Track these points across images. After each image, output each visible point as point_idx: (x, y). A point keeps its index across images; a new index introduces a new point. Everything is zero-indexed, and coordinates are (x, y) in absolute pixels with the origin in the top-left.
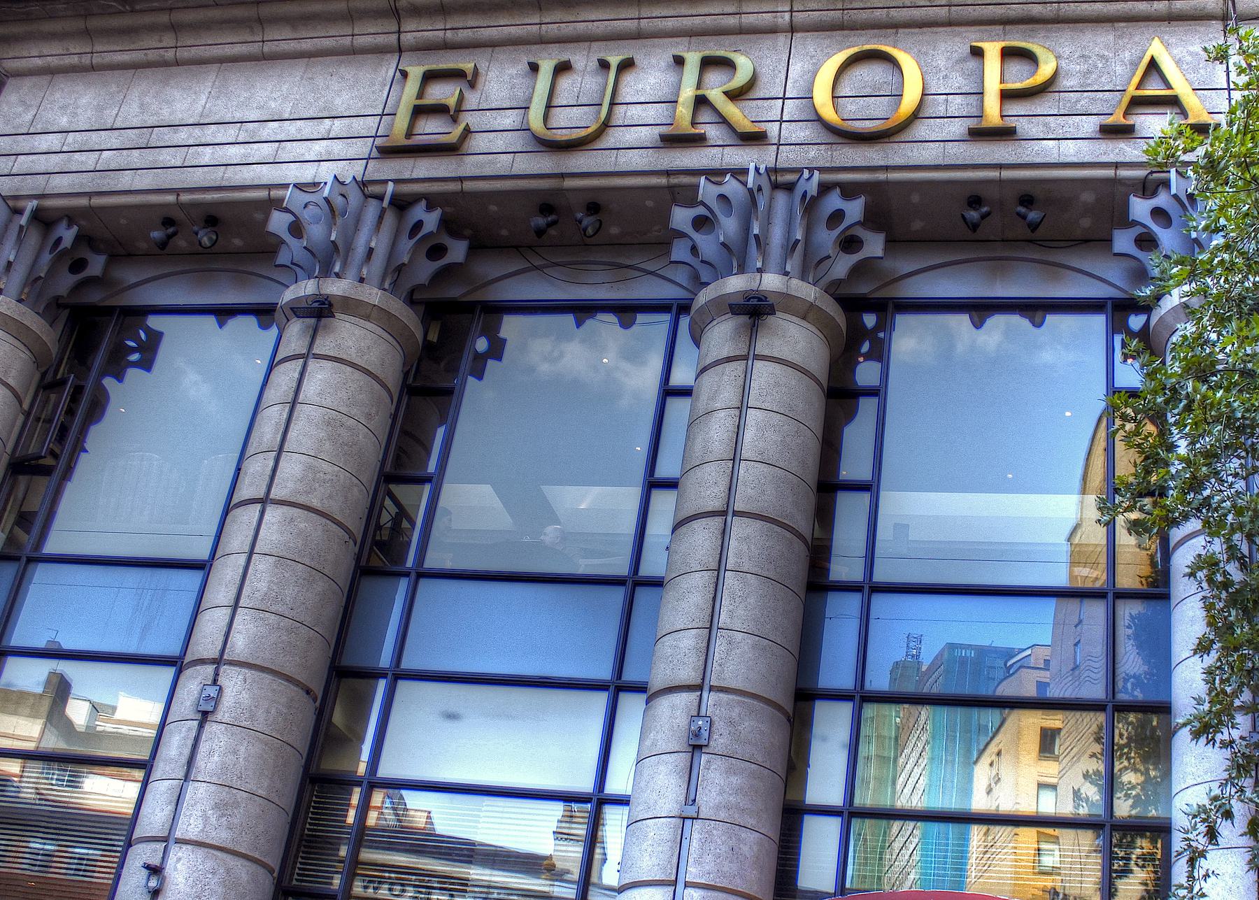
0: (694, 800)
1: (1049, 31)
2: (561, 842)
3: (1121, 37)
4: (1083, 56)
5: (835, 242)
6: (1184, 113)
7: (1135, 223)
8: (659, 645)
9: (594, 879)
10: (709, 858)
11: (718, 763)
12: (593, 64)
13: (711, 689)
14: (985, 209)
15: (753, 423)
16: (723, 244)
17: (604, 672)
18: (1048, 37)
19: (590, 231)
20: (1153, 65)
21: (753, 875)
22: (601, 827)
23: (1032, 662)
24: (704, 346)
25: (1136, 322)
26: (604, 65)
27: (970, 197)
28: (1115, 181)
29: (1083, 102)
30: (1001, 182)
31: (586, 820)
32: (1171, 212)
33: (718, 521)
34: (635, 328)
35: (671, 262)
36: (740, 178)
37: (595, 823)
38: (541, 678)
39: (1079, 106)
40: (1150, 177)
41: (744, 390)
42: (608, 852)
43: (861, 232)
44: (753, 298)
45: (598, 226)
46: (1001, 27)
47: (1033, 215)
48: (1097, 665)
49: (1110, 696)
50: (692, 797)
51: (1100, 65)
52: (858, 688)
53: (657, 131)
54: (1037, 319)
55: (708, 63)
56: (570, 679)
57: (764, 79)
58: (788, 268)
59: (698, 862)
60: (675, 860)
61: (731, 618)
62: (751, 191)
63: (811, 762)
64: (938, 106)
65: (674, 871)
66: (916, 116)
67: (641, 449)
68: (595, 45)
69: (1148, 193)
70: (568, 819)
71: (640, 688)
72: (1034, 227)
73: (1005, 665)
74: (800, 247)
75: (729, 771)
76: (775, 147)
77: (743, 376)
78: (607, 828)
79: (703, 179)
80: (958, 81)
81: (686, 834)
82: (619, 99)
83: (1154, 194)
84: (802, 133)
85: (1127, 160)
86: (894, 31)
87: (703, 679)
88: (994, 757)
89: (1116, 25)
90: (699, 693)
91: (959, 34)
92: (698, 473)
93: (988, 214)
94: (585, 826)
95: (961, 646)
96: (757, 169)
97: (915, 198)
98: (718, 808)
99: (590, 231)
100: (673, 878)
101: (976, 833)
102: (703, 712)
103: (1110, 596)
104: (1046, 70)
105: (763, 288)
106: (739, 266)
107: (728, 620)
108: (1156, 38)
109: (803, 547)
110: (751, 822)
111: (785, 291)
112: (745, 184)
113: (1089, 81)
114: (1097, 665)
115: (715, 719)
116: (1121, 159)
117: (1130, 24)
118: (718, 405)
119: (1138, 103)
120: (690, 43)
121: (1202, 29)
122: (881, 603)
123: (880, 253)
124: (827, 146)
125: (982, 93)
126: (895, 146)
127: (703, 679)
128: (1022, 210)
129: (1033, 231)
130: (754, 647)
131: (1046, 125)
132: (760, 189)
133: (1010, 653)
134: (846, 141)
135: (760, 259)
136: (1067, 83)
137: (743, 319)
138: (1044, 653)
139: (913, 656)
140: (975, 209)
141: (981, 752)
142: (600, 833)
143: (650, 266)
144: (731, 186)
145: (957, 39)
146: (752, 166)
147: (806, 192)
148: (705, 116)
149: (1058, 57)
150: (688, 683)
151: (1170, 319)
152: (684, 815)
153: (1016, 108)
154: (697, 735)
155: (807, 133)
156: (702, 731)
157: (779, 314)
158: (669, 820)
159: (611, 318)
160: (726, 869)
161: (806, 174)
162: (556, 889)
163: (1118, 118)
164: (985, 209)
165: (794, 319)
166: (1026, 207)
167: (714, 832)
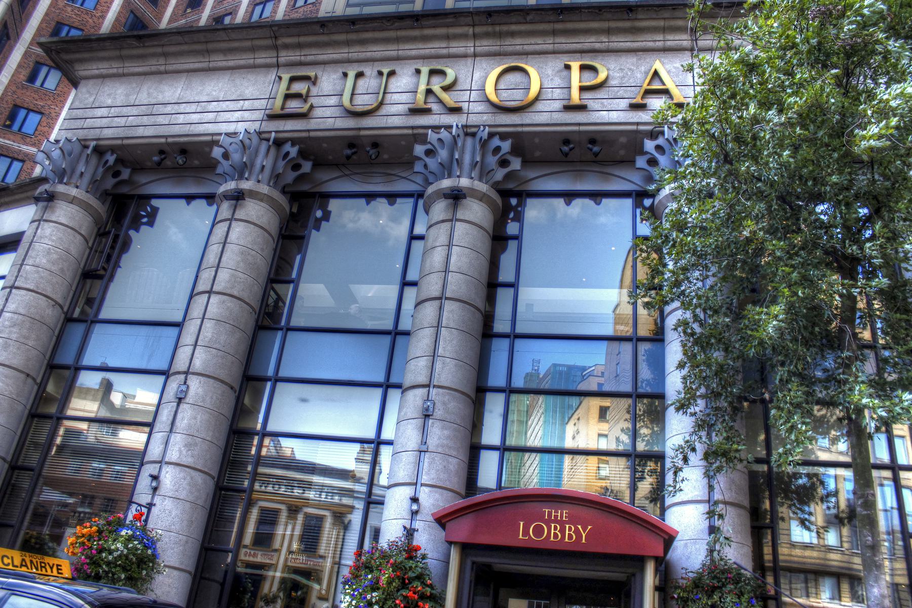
1: (603, 56)
3: (640, 59)
4: (621, 69)
6: (671, 98)
7: (647, 153)
9: (375, 482)
10: (433, 472)
11: (438, 424)
12: (375, 73)
13: (434, 386)
14: (572, 146)
16: (440, 163)
19: (373, 157)
20: (656, 73)
21: (455, 480)
26: (380, 73)
28: (637, 132)
30: (580, 132)
33: (437, 303)
37: (376, 454)
43: (509, 157)
47: (596, 149)
53: (407, 106)
54: (598, 201)
55: (432, 72)
57: (461, 81)
58: (473, 175)
59: (428, 474)
61: (444, 351)
62: (454, 137)
66: (537, 99)
67: (399, 266)
68: (376, 63)
71: (398, 386)
72: (596, 155)
74: (479, 165)
75: (443, 428)
78: (382, 456)
79: (430, 131)
81: (422, 459)
82: (388, 91)
85: (643, 121)
88: (576, 421)
91: (558, 58)
93: (573, 148)
95: (560, 365)
96: (457, 126)
97: (537, 140)
98: (437, 446)
99: (373, 157)
101: (567, 458)
102: (430, 398)
104: (602, 76)
105: (460, 185)
108: (658, 61)
110: (454, 453)
112: (451, 133)
122: (519, 343)
126: (527, 114)
128: (590, 146)
130: (456, 365)
131: (602, 103)
132: (458, 136)
133: (584, 369)
137: (450, 201)
138: (601, 369)
140: (567, 146)
141: (570, 419)
143: (403, 175)
144: (444, 134)
147: (481, 137)
148: (431, 99)
149: (608, 70)
151: (664, 201)
154: (427, 409)
157: (468, 198)
159: (384, 200)
160: (441, 477)
161: (482, 128)
162: (356, 487)
163: (638, 100)
164: (572, 146)
165: (476, 201)
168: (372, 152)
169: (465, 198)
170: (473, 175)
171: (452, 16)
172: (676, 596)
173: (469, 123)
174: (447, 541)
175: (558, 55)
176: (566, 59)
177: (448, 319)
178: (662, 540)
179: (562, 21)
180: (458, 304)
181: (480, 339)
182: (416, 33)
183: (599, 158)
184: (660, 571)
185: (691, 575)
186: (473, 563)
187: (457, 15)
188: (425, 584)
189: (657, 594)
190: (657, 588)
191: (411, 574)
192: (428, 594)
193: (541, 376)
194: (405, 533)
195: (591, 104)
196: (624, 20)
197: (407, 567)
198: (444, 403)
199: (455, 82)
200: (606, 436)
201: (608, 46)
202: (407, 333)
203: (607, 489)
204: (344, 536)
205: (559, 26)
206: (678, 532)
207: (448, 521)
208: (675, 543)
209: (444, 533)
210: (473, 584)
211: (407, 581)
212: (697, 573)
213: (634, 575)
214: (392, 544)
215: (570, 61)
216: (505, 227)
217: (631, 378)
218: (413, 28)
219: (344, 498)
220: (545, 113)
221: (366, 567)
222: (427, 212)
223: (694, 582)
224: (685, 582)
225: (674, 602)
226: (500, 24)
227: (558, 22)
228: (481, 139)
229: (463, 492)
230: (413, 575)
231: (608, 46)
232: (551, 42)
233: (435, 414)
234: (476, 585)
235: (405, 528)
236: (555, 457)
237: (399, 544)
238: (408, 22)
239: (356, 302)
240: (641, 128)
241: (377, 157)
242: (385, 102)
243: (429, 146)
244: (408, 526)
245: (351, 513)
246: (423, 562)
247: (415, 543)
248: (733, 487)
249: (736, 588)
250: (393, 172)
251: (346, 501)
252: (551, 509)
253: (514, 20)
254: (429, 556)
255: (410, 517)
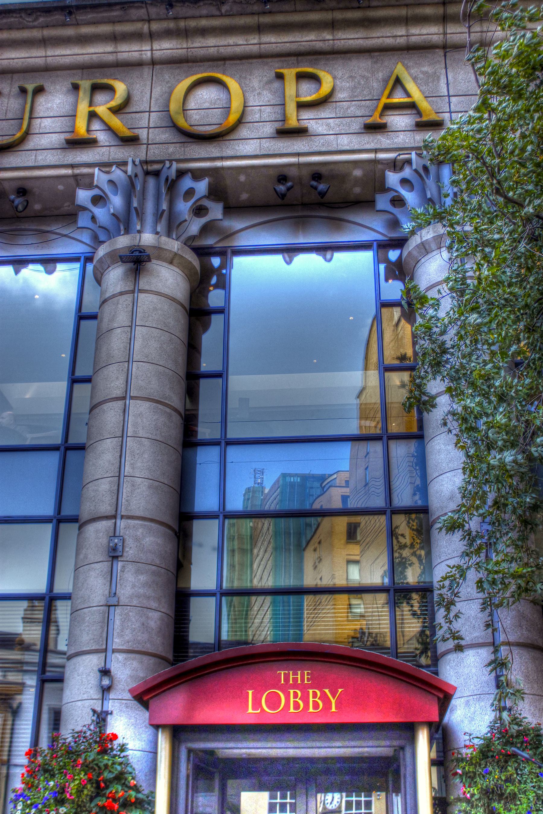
0: (115, 594)
1: (328, 59)
2: (28, 624)
3: (376, 62)
4: (351, 77)
5: (189, 211)
6: (419, 113)
7: (390, 189)
8: (85, 490)
9: (51, 646)
10: (128, 632)
11: (130, 567)
12: (15, 90)
13: (122, 517)
14: (289, 184)
15: (140, 336)
16: (113, 215)
17: (48, 510)
18: (327, 64)
19: (20, 208)
20: (398, 81)
21: (158, 640)
22: (53, 612)
23: (338, 482)
24: (104, 285)
25: (393, 255)
26: (23, 91)
27: (279, 176)
28: (375, 162)
29: (352, 109)
30: (299, 165)
31: (43, 608)
32: (413, 181)
33: (120, 403)
34: (55, 274)
35: (78, 228)
36: (123, 168)
37: (49, 611)
38: (5, 517)
39: (349, 111)
40: (398, 158)
41: (133, 314)
42: (61, 628)
43: (207, 203)
44: (136, 251)
45: (25, 204)
46: (295, 58)
47: (322, 187)
48: (378, 484)
49: (388, 505)
50: (113, 591)
51: (363, 83)
52: (222, 510)
53: (63, 137)
54: (328, 256)
55: (96, 88)
56: (25, 517)
57: (136, 97)
58: (159, 229)
59: (121, 636)
60: (105, 635)
61: (133, 468)
62: (130, 177)
63: (193, 561)
64: (254, 115)
65: (105, 642)
66: (240, 122)
67: (66, 356)
68: (16, 76)
69: (398, 168)
70: (30, 608)
71: (74, 519)
72: (322, 194)
73: (321, 485)
74: (166, 214)
75: (138, 572)
76: (145, 146)
77: (131, 304)
78: (58, 612)
79: (96, 170)
80: (267, 96)
81: (111, 617)
82: (36, 115)
83: (401, 169)
84: (165, 136)
85: (383, 147)
86: (223, 62)
87: (116, 511)
88: (316, 545)
89: (372, 54)
90: (114, 521)
91: (267, 64)
92: (105, 371)
93: (292, 187)
94: (42, 612)
95: (290, 475)
96: (134, 162)
97: (242, 178)
98: (131, 597)
99: (20, 208)
100: (104, 647)
101: (308, 600)
102: (117, 534)
103: (385, 438)
104: (326, 88)
105: (142, 243)
106: (125, 229)
107: (131, 470)
108: (400, 63)
109: (179, 417)
110: (154, 605)
111: (157, 245)
112: (126, 172)
113: (356, 94)
114: (378, 484)
115: (126, 537)
116: (378, 146)
117: (382, 53)
118: (116, 325)
119: (388, 107)
120: (82, 74)
121: (430, 56)
122: (233, 453)
123: (219, 216)
124: (180, 145)
125: (284, 104)
126: (227, 143)
127: (116, 511)
128: (314, 183)
129: (322, 198)
130: (150, 487)
131: (328, 125)
132: (136, 176)
133: (322, 478)
134: (194, 140)
135: (139, 224)
136: (340, 95)
137: (131, 265)
138: (344, 476)
139: (258, 484)
140: (283, 184)
141: (308, 543)
142: (53, 616)
143: (65, 232)
144: (117, 174)
145: (266, 68)
146: (130, 160)
147: (168, 177)
148: (96, 126)
149: (334, 78)
150: (106, 514)
151: (415, 253)
152: (109, 604)
153: (306, 115)
154: (115, 549)
155: (167, 135)
156: (118, 546)
157: (154, 261)
158: (99, 608)
159: (40, 267)
160: (139, 638)
161: (167, 164)
162: (26, 657)
163: (376, 119)
164: (289, 184)
165: (164, 264)
166: (317, 181)
167: (131, 614)
168: (19, 201)
169: (150, 261)
170: (159, 229)
171: (118, 7)
172: (460, 771)
173: (151, 158)
174: (152, 725)
175: (265, 60)
176: (277, 65)
177: (135, 425)
178: (436, 698)
179: (270, 12)
180: (147, 404)
181: (180, 449)
182: (70, 32)
183: (328, 198)
184: (435, 739)
185: (476, 741)
186: (190, 751)
187: (126, 6)
188: (127, 786)
189: (434, 769)
190: (433, 763)
191: (106, 775)
192: (133, 799)
193: (266, 491)
194: (94, 718)
195: (313, 126)
196: (353, 8)
197: (101, 765)
198: (137, 539)
199: (127, 101)
200: (357, 562)
201: (334, 45)
202: (82, 448)
203: (363, 633)
204: (13, 725)
205: (266, 19)
206: (455, 689)
207: (151, 698)
208: (454, 702)
209: (147, 714)
210: (191, 779)
211: (103, 785)
212: (485, 739)
213: (402, 748)
214: (79, 735)
215: (282, 68)
216: (207, 297)
217: (383, 496)
218: (64, 25)
219: (9, 674)
220: (252, 141)
221: (46, 771)
222: (99, 281)
223: (482, 752)
224: (469, 751)
225: (458, 780)
226: (185, 18)
227: (264, 13)
228: (167, 179)
229: (170, 657)
230: (111, 776)
231: (334, 45)
232: (255, 41)
233: (125, 554)
234: (196, 778)
235: (94, 711)
236: (292, 598)
237: (89, 733)
238: (58, 17)
239: (10, 408)
240: (382, 156)
241: (25, 208)
242: (32, 131)
243: (96, 192)
244: (99, 709)
245: (20, 693)
246: (122, 755)
247: (109, 731)
248: (524, 623)
249: (535, 754)
250: (48, 229)
251: (12, 677)
252: (289, 670)
253: (204, 12)
254: (129, 746)
255: (100, 696)
